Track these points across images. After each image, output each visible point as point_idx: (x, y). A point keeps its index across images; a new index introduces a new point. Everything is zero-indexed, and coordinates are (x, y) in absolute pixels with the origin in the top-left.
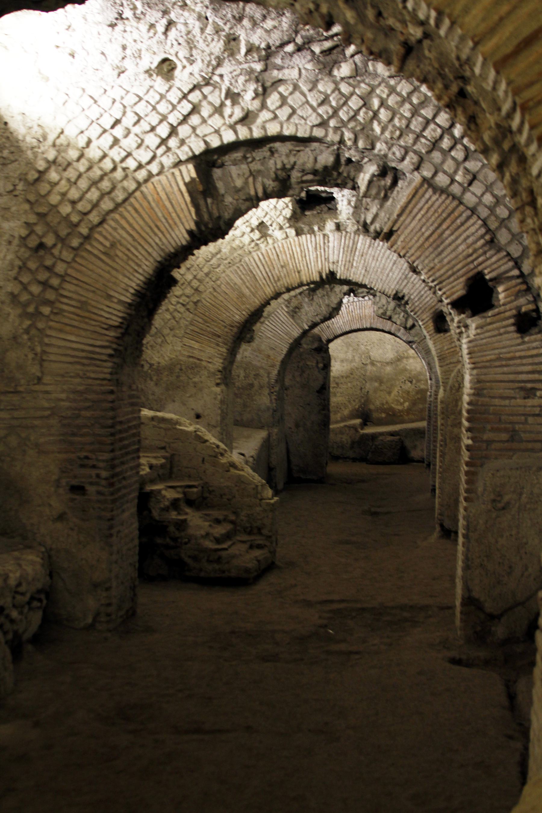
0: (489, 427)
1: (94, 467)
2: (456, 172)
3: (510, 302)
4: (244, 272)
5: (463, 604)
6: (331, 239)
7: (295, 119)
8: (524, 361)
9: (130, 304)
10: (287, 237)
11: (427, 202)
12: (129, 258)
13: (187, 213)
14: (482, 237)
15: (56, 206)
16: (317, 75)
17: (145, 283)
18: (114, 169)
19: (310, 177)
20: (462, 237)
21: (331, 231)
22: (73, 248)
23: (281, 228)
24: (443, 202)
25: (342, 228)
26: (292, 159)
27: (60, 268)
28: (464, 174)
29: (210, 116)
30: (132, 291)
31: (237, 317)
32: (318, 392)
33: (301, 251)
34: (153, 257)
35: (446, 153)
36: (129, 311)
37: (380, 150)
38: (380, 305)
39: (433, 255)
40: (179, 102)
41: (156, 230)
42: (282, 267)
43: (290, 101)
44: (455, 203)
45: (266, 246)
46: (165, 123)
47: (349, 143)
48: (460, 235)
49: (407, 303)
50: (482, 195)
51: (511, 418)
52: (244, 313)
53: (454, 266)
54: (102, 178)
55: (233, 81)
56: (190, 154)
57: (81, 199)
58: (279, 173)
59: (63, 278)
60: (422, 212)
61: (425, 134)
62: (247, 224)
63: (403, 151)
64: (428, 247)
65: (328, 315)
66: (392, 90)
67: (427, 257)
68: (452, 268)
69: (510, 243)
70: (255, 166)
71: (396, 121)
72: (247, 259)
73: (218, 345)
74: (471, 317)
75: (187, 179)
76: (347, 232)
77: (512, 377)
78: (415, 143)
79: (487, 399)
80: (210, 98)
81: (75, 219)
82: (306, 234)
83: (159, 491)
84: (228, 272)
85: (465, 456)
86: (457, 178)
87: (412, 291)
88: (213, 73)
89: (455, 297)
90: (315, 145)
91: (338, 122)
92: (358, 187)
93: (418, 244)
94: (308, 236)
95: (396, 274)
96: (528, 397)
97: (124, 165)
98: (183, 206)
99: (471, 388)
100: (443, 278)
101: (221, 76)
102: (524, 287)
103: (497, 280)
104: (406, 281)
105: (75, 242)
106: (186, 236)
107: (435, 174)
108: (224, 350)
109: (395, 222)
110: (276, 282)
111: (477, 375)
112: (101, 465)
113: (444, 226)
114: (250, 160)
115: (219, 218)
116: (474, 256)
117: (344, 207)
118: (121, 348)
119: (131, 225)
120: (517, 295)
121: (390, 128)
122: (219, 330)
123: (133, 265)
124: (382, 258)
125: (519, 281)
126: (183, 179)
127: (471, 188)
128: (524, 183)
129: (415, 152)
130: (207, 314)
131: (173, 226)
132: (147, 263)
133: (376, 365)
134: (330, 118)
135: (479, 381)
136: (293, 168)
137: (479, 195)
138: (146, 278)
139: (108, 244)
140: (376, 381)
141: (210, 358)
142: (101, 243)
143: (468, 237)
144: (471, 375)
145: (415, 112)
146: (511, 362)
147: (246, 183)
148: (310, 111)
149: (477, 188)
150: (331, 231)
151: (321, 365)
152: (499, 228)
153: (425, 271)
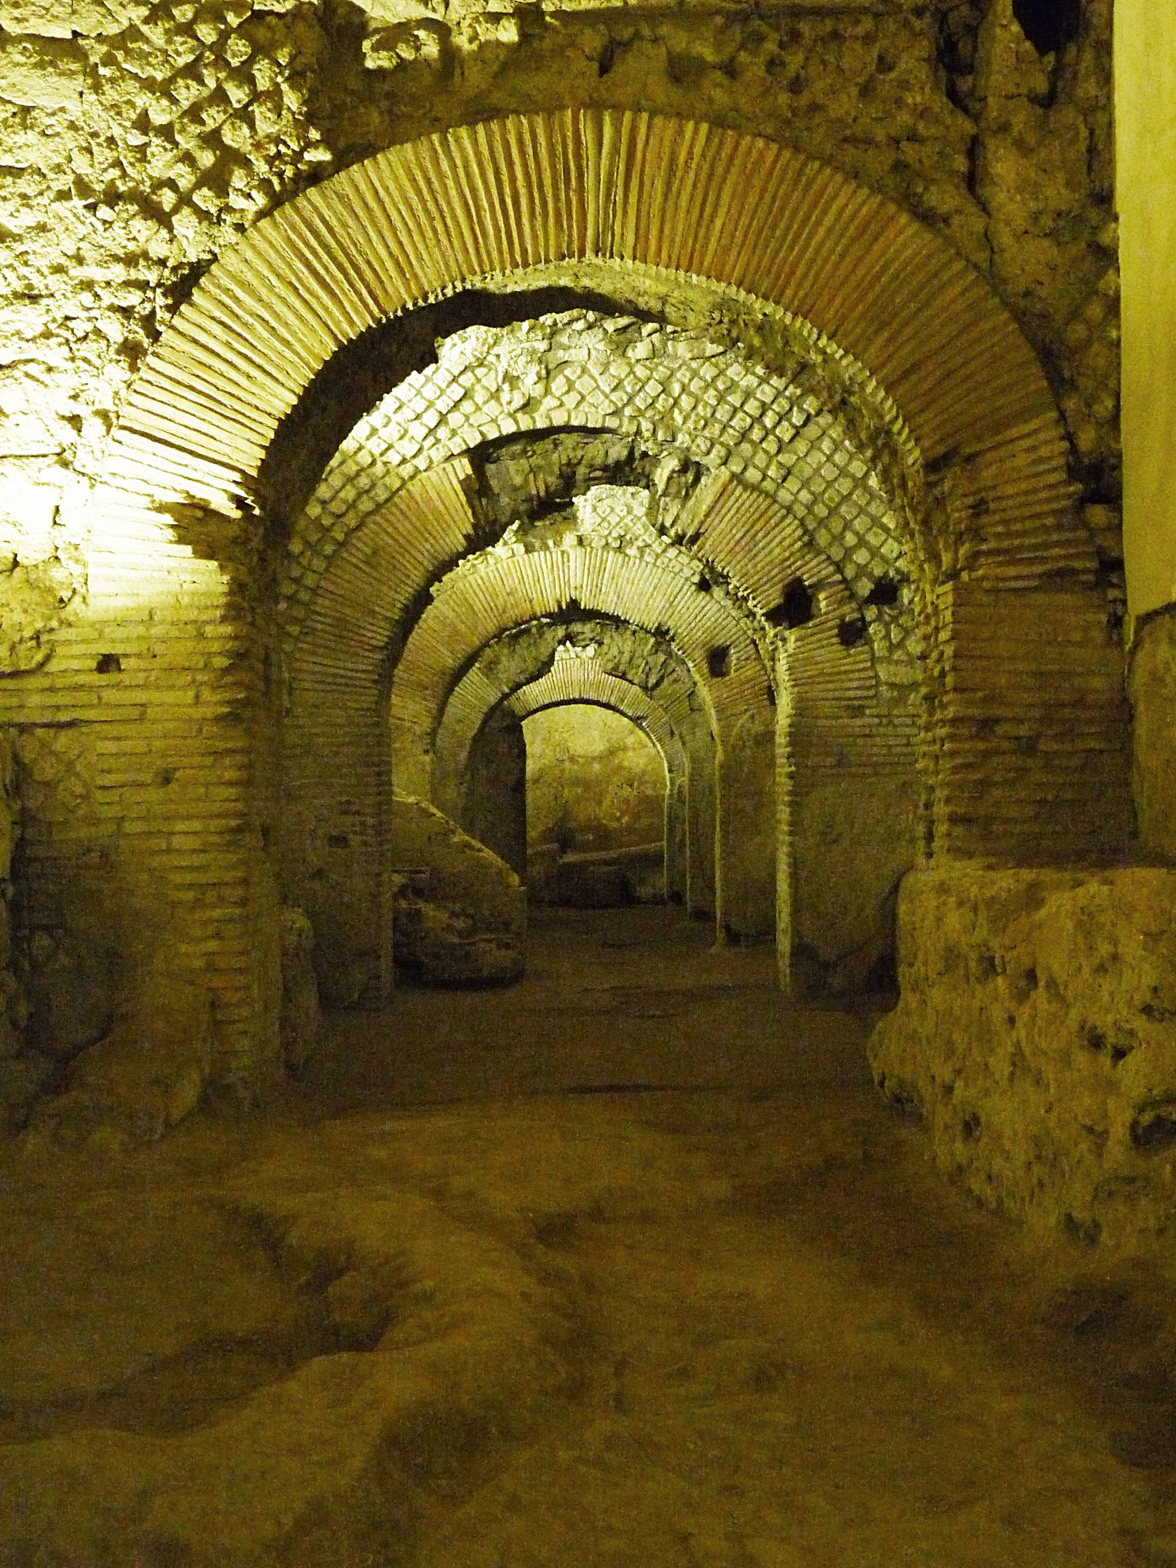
1: (358, 813)
2: (768, 467)
7: (584, 407)
9: (397, 621)
13: (462, 514)
14: (800, 539)
16: (608, 357)
17: (414, 596)
18: (373, 463)
19: (598, 473)
20: (777, 540)
21: (571, 547)
22: (326, 557)
26: (579, 453)
27: (310, 580)
29: (485, 403)
35: (756, 445)
38: (609, 656)
40: (448, 386)
42: (508, 594)
43: (577, 385)
44: (769, 501)
46: (432, 410)
47: (647, 434)
49: (672, 639)
53: (770, 571)
54: (358, 474)
55: (512, 362)
56: (464, 447)
57: (333, 498)
58: (564, 468)
59: (315, 591)
61: (732, 423)
66: (695, 374)
69: (830, 545)
70: (535, 461)
71: (700, 408)
72: (461, 585)
73: (425, 699)
74: (790, 628)
75: (462, 476)
78: (721, 435)
80: (484, 381)
81: (327, 521)
86: (769, 473)
88: (488, 353)
89: (772, 605)
92: (654, 485)
93: (729, 548)
94: (542, 553)
95: (658, 600)
97: (384, 459)
98: (458, 506)
101: (498, 356)
102: (847, 593)
103: (819, 586)
105: (329, 549)
106: (463, 541)
107: (745, 469)
108: (433, 706)
109: (702, 523)
111: (798, 692)
112: (368, 811)
113: (757, 528)
116: (792, 560)
117: (587, 515)
120: (841, 602)
121: (693, 416)
122: (426, 680)
123: (399, 575)
125: (842, 586)
128: (895, 471)
129: (722, 444)
133: (578, 762)
134: (625, 406)
136: (579, 463)
137: (795, 491)
139: (369, 552)
140: (578, 786)
141: (414, 717)
145: (721, 399)
147: (526, 480)
148: (602, 398)
149: (792, 484)
150: (571, 547)
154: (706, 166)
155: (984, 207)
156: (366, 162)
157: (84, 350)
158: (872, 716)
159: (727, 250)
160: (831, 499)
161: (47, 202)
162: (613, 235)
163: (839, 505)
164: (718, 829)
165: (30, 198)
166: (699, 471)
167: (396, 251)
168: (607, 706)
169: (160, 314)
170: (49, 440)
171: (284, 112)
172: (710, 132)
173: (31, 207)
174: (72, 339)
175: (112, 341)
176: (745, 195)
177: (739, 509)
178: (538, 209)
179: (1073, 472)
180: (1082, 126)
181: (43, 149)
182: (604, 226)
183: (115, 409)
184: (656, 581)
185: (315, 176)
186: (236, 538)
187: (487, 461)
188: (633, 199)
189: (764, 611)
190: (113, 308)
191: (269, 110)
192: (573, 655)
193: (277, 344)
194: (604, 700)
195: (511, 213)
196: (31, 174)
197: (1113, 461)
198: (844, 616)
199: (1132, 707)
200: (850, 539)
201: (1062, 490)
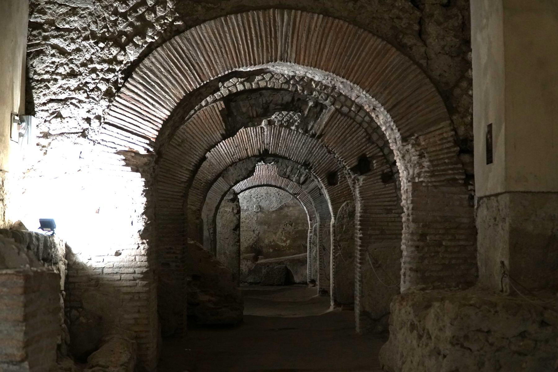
1: (174, 253)
2: (351, 106)
3: (378, 168)
5: (360, 315)
9: (192, 171)
11: (338, 120)
12: (191, 148)
14: (365, 137)
20: (355, 137)
24: (346, 120)
25: (272, 123)
26: (271, 98)
28: (356, 107)
30: (193, 164)
31: (209, 177)
32: (234, 230)
33: (247, 137)
37: (315, 95)
39: (341, 146)
41: (205, 134)
44: (352, 121)
48: (354, 137)
50: (364, 117)
52: (214, 175)
58: (264, 105)
60: (336, 125)
63: (326, 96)
65: (246, 176)
68: (351, 152)
69: (378, 140)
70: (253, 102)
73: (197, 194)
75: (220, 109)
76: (275, 126)
79: (369, 215)
82: (250, 127)
85: (359, 242)
86: (352, 109)
87: (315, 160)
89: (353, 165)
90: (282, 92)
91: (294, 82)
96: (389, 213)
99: (361, 209)
102: (385, 161)
103: (373, 157)
106: (220, 137)
107: (342, 107)
110: (232, 156)
111: (364, 203)
113: (347, 132)
114: (250, 98)
120: (382, 165)
124: (296, 141)
126: (218, 108)
127: (359, 114)
129: (333, 96)
131: (214, 132)
132: (201, 150)
135: (365, 206)
136: (271, 102)
139: (180, 141)
140: (265, 225)
143: (358, 137)
144: (361, 203)
146: (380, 197)
151: (235, 211)
152: (373, 133)
153: (338, 153)
154: (321, 30)
155: (425, 45)
156: (197, 27)
157: (93, 95)
158: (395, 213)
159: (329, 60)
161: (80, 41)
162: (287, 54)
164: (331, 255)
165: (74, 39)
166: (323, 107)
167: (207, 59)
168: (280, 188)
169: (119, 81)
170: (79, 127)
171: (167, 8)
172: (323, 18)
173: (75, 43)
174: (88, 90)
175: (102, 91)
176: (336, 39)
177: (339, 124)
178: (260, 45)
179: (457, 142)
180: (460, 14)
181: (80, 22)
182: (284, 51)
183: (103, 116)
185: (179, 31)
186: (146, 163)
187: (231, 101)
188: (295, 42)
189: (349, 168)
190: (103, 79)
191: (162, 8)
193: (163, 93)
194: (279, 185)
195: (250, 46)
196: (75, 31)
197: (471, 138)
198: (384, 170)
199: (477, 230)
201: (452, 150)
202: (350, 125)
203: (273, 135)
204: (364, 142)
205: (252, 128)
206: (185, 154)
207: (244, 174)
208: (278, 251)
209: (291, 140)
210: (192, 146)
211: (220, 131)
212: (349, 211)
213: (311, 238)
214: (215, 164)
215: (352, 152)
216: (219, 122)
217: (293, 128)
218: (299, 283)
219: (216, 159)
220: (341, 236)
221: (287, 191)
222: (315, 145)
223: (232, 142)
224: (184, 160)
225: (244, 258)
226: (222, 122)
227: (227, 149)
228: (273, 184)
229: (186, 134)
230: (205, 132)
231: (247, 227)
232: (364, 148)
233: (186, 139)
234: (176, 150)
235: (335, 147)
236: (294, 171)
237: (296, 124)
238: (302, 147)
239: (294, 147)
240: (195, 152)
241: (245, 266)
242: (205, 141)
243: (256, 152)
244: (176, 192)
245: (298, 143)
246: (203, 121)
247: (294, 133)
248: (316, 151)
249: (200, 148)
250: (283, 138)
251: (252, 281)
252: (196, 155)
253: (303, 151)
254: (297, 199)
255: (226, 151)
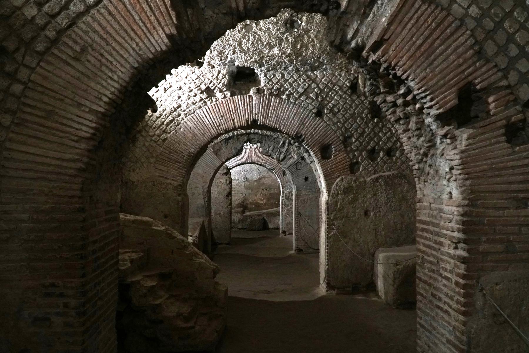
0: (484, 239)
1: (61, 295)
3: (500, 112)
4: (197, 120)
6: (254, 98)
8: (516, 171)
10: (225, 97)
12: (102, 64)
14: (471, 47)
15: (20, 8)
20: (452, 47)
22: (38, 53)
23: (221, 91)
24: (432, 12)
25: (260, 92)
30: (105, 99)
31: (193, 150)
32: (226, 196)
33: (234, 106)
34: (129, 63)
36: (103, 122)
39: (425, 65)
41: (132, 34)
44: (444, 13)
45: (211, 103)
48: (450, 46)
50: (469, 7)
51: (505, 228)
52: (197, 147)
62: (198, 88)
64: (420, 57)
67: (419, 67)
68: (444, 78)
69: (496, 54)
73: (179, 168)
74: (459, 128)
76: (264, 94)
77: (504, 187)
83: (138, 282)
84: (186, 119)
87: (307, 132)
100: (435, 88)
103: (487, 90)
104: (303, 126)
105: (40, 47)
106: (166, 40)
110: (218, 127)
111: (470, 185)
113: (434, 36)
115: (199, 29)
118: (94, 162)
119: (104, 28)
120: (507, 106)
124: (287, 111)
130: (172, 147)
131: (152, 31)
132: (123, 70)
135: (472, 192)
138: (121, 85)
139: (78, 49)
140: (249, 189)
141: (174, 177)
142: (71, 48)
143: (458, 47)
146: (503, 172)
151: (228, 182)
152: (485, 39)
160: (496, 15)
163: (502, 21)
168: (261, 165)
177: (419, 18)
184: (295, 111)
192: (249, 147)
194: (260, 163)
200: (514, 51)
202: (442, 22)
203: (262, 105)
204: (471, 58)
205: (239, 97)
206: (88, 77)
207: (234, 152)
208: (258, 206)
209: (282, 110)
210: (104, 60)
211: (165, 28)
212: (344, 186)
213: (283, 201)
214: (199, 135)
215: (447, 79)
216: (163, 9)
217: (284, 97)
218: (272, 229)
219: (199, 130)
220: (336, 214)
221: (266, 167)
222: (308, 115)
223: (218, 111)
224: (85, 91)
225: (236, 212)
226: (170, 9)
227: (212, 119)
228: (256, 162)
229: (91, 34)
230: (133, 30)
231: (237, 191)
232: (470, 70)
233: (91, 46)
234: (68, 69)
235: (410, 67)
236: (275, 150)
237: (287, 92)
238: (293, 119)
239: (285, 117)
240: (110, 74)
241: (236, 217)
242: (134, 49)
243: (244, 123)
244: (68, 160)
245: (289, 114)
246: (128, 6)
247: (285, 103)
248: (308, 122)
249: (122, 65)
250: (272, 107)
251: (241, 227)
252: (112, 79)
253: (294, 121)
254: (273, 173)
255: (211, 122)
